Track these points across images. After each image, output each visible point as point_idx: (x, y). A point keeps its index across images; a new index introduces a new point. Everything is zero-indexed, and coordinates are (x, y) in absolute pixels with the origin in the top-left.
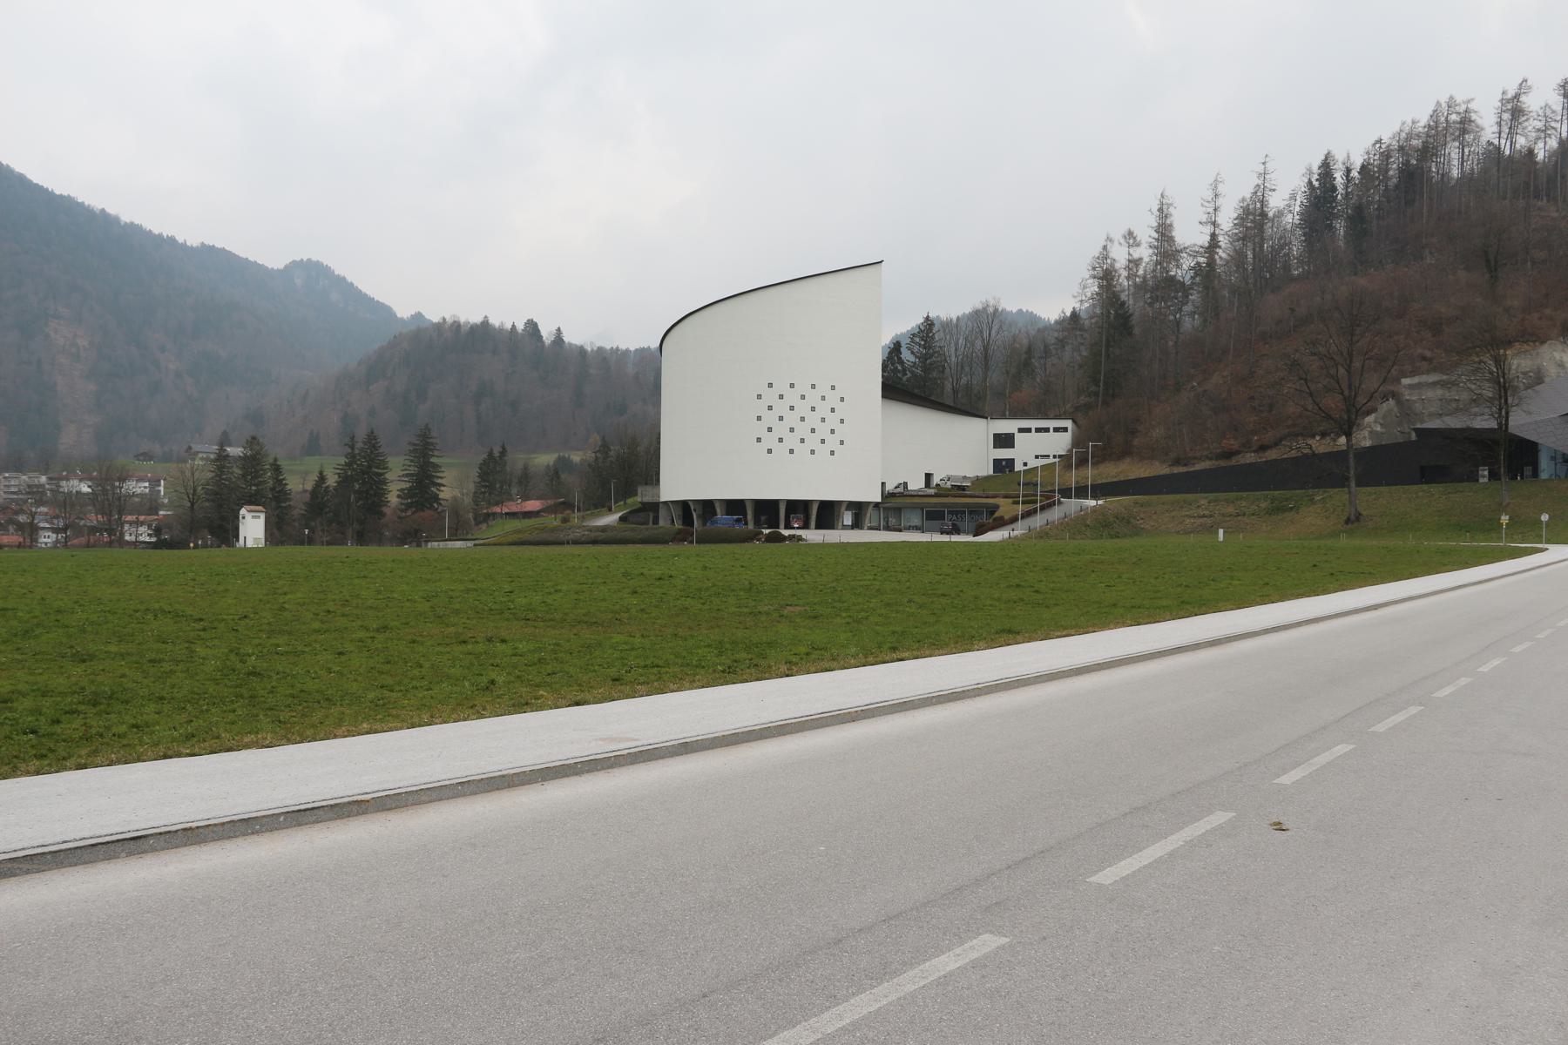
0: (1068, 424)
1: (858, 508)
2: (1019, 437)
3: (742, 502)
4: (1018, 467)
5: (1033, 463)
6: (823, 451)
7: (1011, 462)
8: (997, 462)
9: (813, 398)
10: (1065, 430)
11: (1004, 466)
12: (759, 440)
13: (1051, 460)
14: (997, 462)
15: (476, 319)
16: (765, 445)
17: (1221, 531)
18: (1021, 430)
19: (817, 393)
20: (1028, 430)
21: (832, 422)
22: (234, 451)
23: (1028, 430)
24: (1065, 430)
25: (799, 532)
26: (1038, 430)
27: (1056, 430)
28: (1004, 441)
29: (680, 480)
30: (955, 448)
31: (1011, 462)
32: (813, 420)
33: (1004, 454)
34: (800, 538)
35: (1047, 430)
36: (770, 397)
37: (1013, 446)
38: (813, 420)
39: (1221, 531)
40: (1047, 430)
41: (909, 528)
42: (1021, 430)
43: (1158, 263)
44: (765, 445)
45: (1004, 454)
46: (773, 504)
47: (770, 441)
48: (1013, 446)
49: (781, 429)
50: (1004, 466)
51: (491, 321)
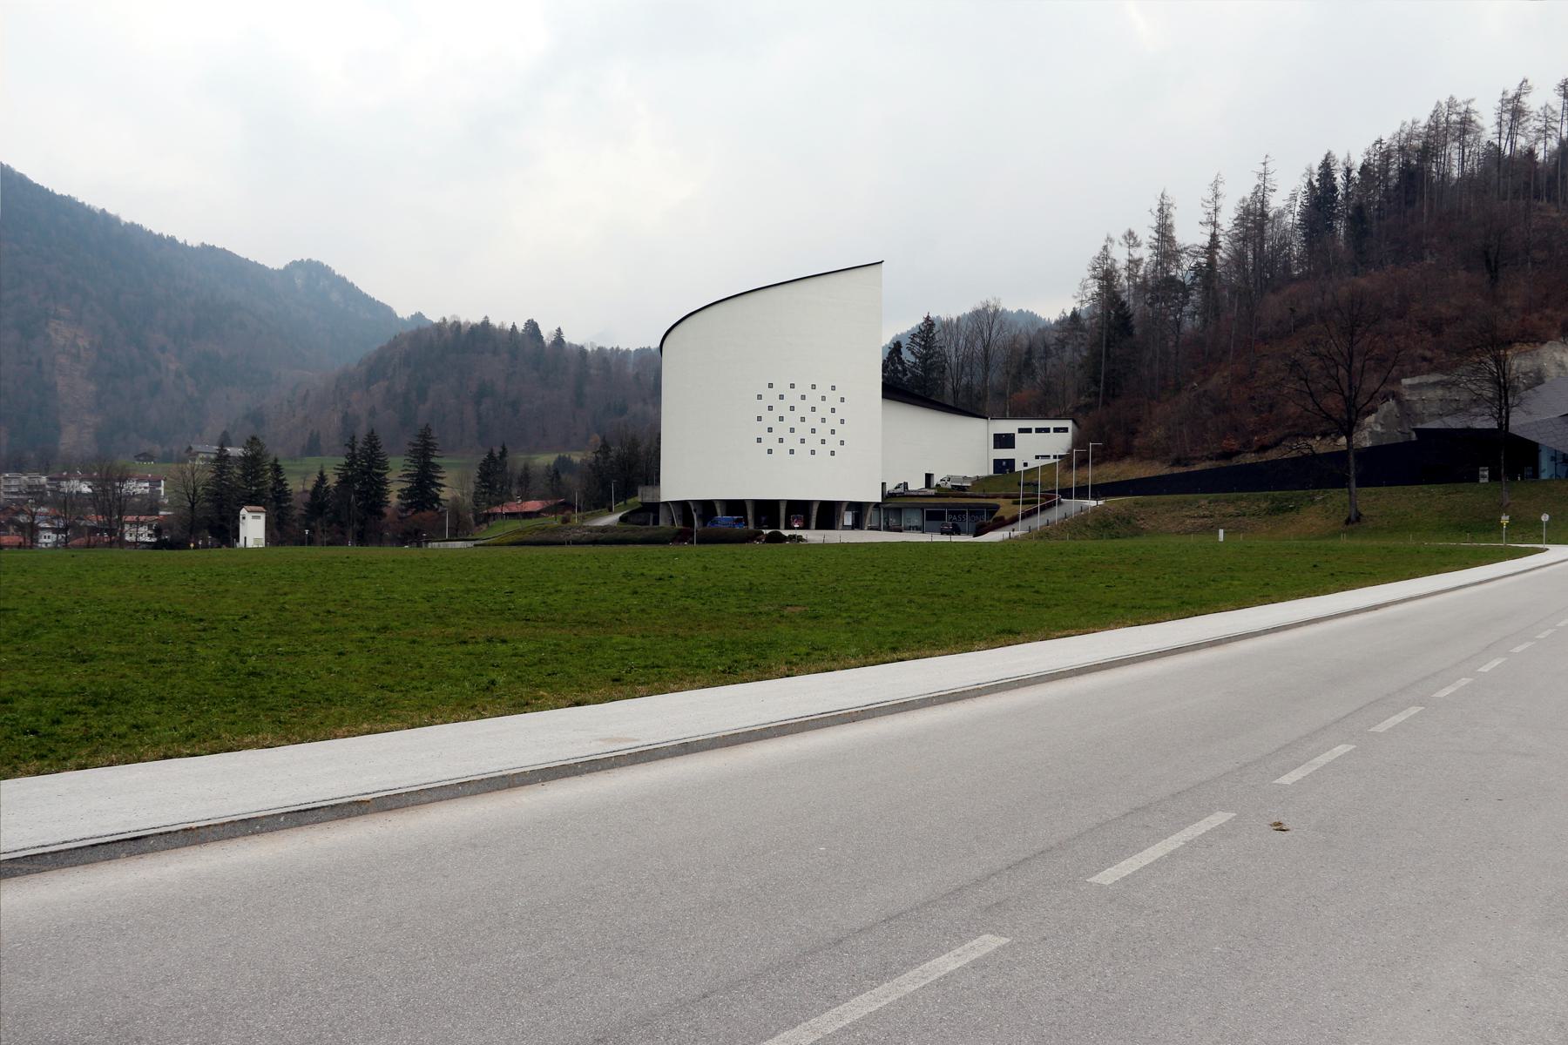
0: (1068, 424)
1: (858, 508)
2: (1019, 438)
4: (1019, 467)
5: (1033, 463)
7: (1011, 462)
8: (997, 463)
10: (1066, 430)
11: (1004, 467)
13: (1052, 460)
14: (997, 463)
18: (1021, 431)
20: (1029, 431)
23: (1029, 431)
24: (1066, 430)
26: (1039, 430)
27: (1057, 430)
28: (1004, 441)
30: (955, 449)
31: (1011, 462)
32: (813, 420)
33: (1004, 454)
34: (800, 539)
35: (1047, 430)
38: (813, 420)
40: (1047, 430)
41: (909, 529)
42: (1021, 431)
44: (765, 391)
45: (1004, 454)
47: (770, 441)
49: (781, 430)
50: (1004, 467)
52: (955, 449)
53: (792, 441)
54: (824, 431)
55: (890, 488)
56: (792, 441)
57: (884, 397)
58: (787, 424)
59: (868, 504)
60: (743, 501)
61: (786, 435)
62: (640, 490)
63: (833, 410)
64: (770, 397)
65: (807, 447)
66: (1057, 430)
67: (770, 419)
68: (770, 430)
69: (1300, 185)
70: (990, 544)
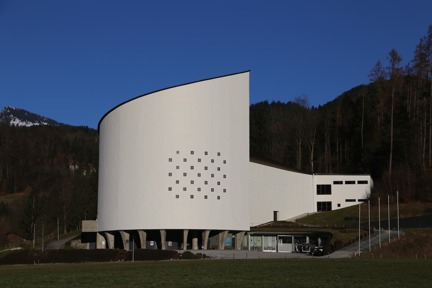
0: (368, 178)
2: (334, 188)
3: (181, 232)
4: (334, 207)
7: (329, 204)
8: (320, 205)
10: (366, 182)
11: (324, 206)
12: (170, 189)
13: (357, 203)
16: (221, 194)
17: (308, 239)
18: (335, 183)
21: (219, 176)
23: (341, 183)
24: (366, 182)
26: (359, 182)
27: (359, 182)
28: (324, 189)
30: (296, 194)
31: (329, 204)
33: (324, 198)
35: (353, 182)
36: (218, 162)
39: (308, 239)
40: (353, 182)
42: (335, 183)
43: (417, 65)
44: (221, 194)
45: (324, 198)
46: (157, 232)
47: (177, 189)
50: (324, 206)
52: (361, 202)
53: (192, 160)
56: (192, 160)
57: (251, 160)
63: (219, 183)
64: (219, 191)
68: (185, 175)
70: (343, 260)
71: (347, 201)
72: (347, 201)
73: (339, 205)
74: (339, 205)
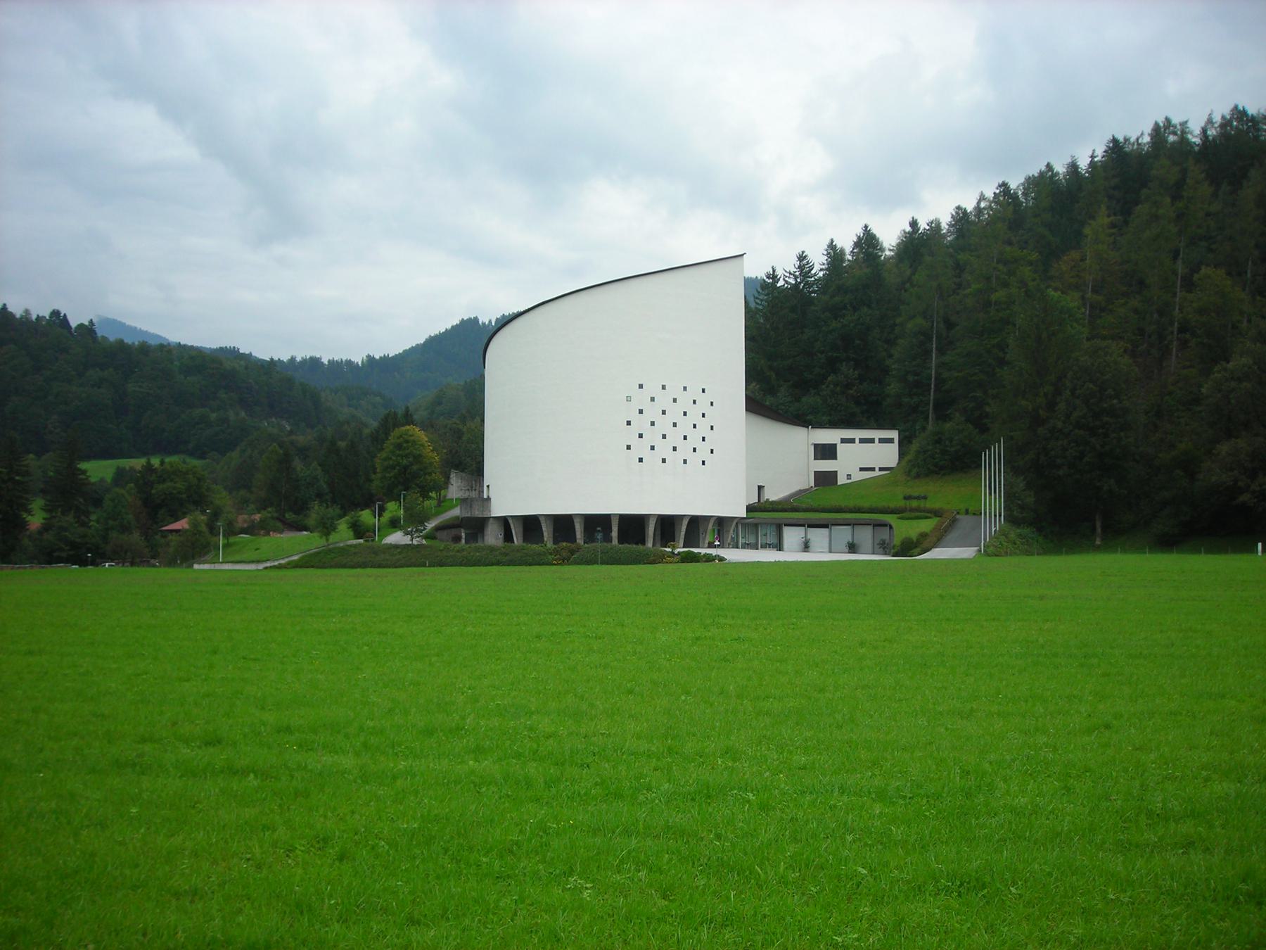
0: (894, 434)
1: (721, 522)
2: (841, 448)
4: (842, 480)
5: (859, 476)
6: (694, 460)
8: (818, 475)
9: (664, 401)
10: (890, 441)
11: (826, 479)
13: (877, 473)
14: (818, 475)
15: (41, 309)
18: (844, 441)
19: (689, 396)
20: (852, 441)
22: (342, 444)
23: (852, 441)
24: (890, 441)
25: (713, 552)
26: (862, 441)
27: (882, 441)
28: (826, 452)
29: (522, 479)
32: (664, 424)
33: (826, 465)
34: (722, 559)
35: (872, 441)
37: (815, 459)
38: (664, 424)
40: (872, 441)
41: (765, 546)
42: (844, 441)
45: (826, 465)
48: (815, 459)
49: (652, 436)
50: (826, 479)
51: (10, 309)
53: (664, 449)
54: (694, 439)
55: (772, 495)
57: (755, 405)
58: (669, 430)
59: (707, 518)
60: (570, 516)
61: (658, 442)
62: (45, 515)
65: (680, 455)
66: (882, 441)
67: (640, 424)
69: (824, 259)
71: (861, 469)
72: (861, 469)
73: (849, 476)
74: (849, 476)
